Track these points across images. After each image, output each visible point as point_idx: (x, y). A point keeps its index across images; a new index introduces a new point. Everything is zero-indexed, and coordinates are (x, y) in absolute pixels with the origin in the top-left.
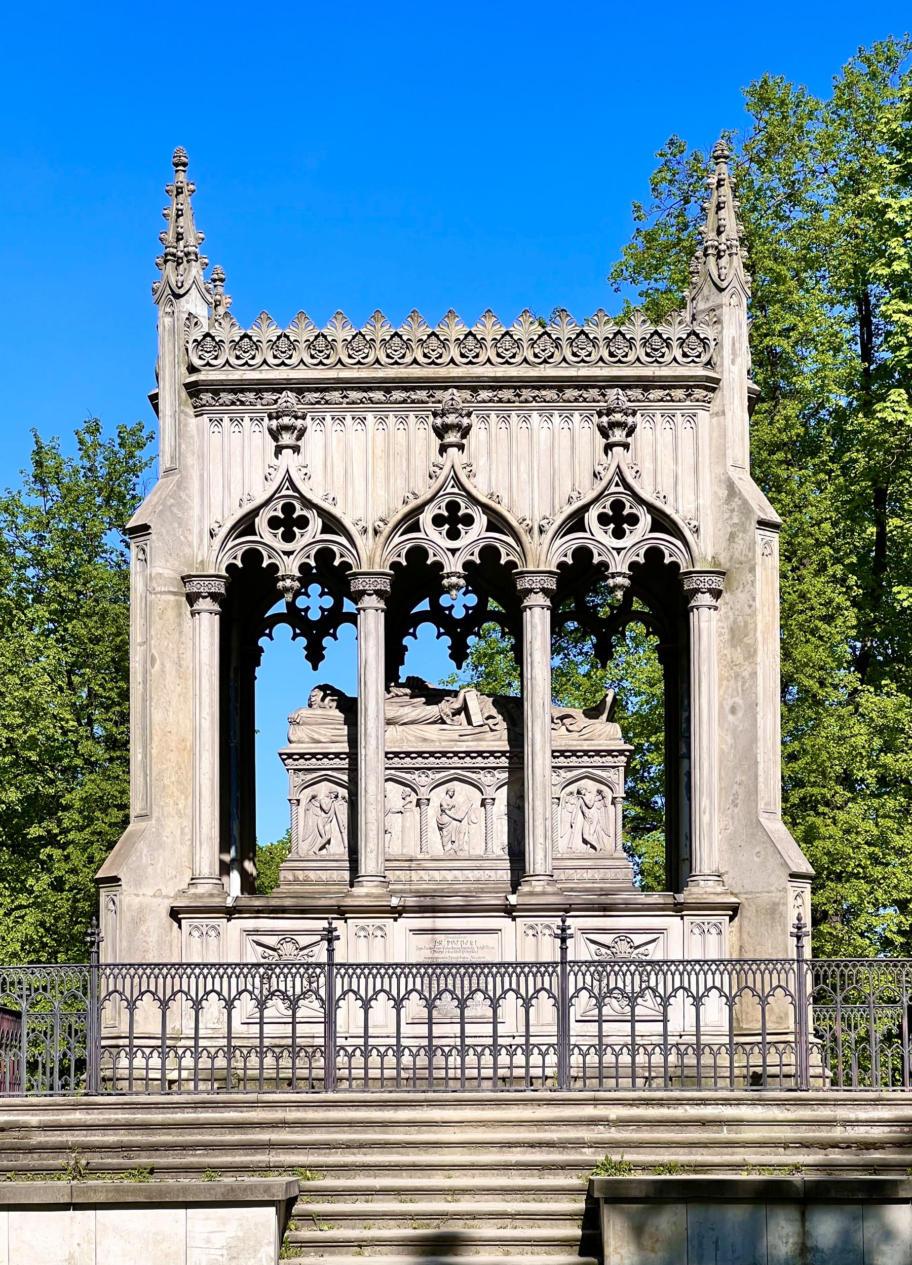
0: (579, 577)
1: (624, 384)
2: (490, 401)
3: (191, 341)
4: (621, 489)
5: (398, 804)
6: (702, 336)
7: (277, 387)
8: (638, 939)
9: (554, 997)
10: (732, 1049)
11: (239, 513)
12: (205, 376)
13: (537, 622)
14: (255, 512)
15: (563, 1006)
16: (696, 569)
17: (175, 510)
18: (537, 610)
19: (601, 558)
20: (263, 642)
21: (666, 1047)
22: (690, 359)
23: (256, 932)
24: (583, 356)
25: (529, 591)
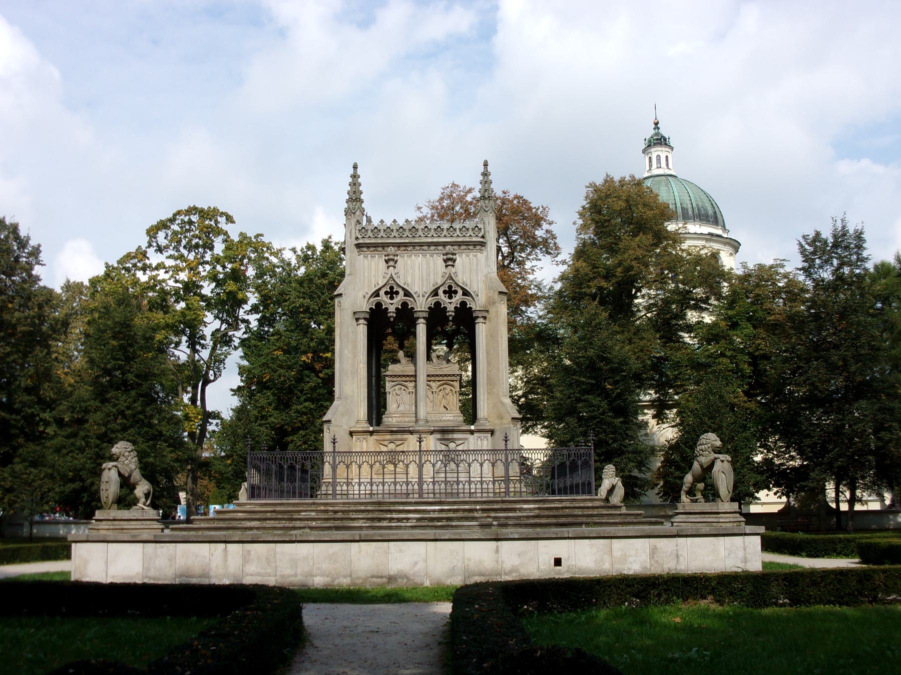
0: (436, 314)
8: (399, 443)
10: (494, 482)
12: (361, 241)
13: (421, 329)
14: (380, 289)
15: (420, 467)
25: (418, 318)
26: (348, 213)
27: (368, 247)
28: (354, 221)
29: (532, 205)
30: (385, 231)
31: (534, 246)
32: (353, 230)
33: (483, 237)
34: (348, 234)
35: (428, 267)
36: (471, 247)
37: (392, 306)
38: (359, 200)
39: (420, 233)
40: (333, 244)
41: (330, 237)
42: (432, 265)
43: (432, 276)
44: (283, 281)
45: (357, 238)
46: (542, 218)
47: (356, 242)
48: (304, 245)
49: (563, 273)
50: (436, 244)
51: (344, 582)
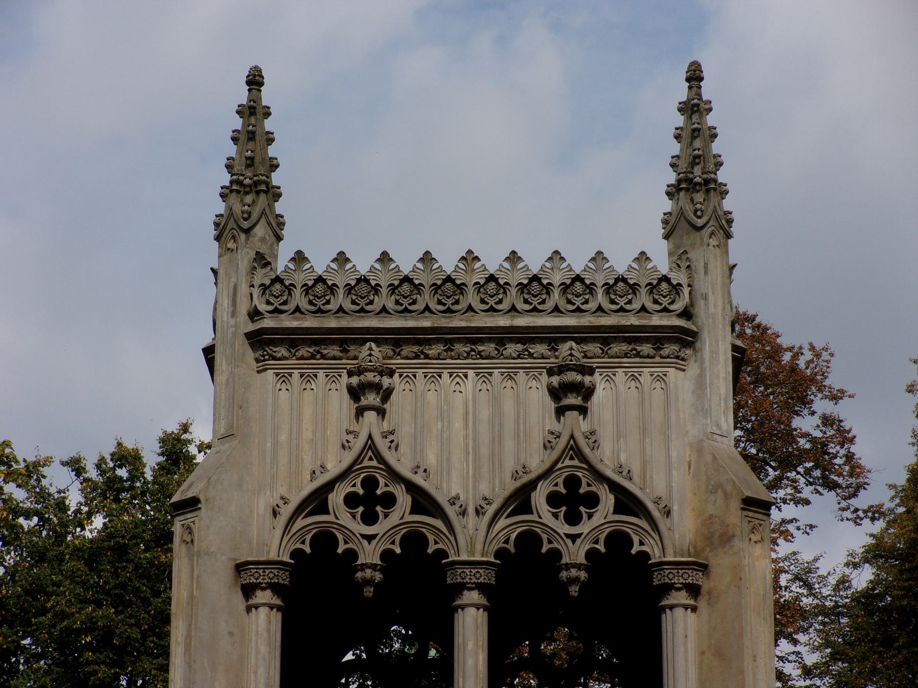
0: (522, 576)
2: (519, 357)
3: (256, 286)
4: (374, 463)
7: (362, 336)
11: (309, 488)
12: (268, 323)
13: (471, 628)
14: (329, 487)
16: (666, 559)
24: (535, 303)
26: (227, 230)
27: (293, 345)
28: (245, 258)
29: (783, 341)
30: (349, 289)
31: (788, 463)
32: (244, 289)
33: (686, 314)
34: (225, 302)
35: (497, 414)
36: (646, 348)
37: (370, 544)
38: (712, 188)
39: (471, 298)
40: (193, 449)
41: (185, 428)
42: (509, 406)
43: (509, 444)
44: (40, 556)
45: (254, 314)
46: (812, 380)
47: (251, 327)
48: (108, 449)
49: (878, 538)
50: (527, 336)
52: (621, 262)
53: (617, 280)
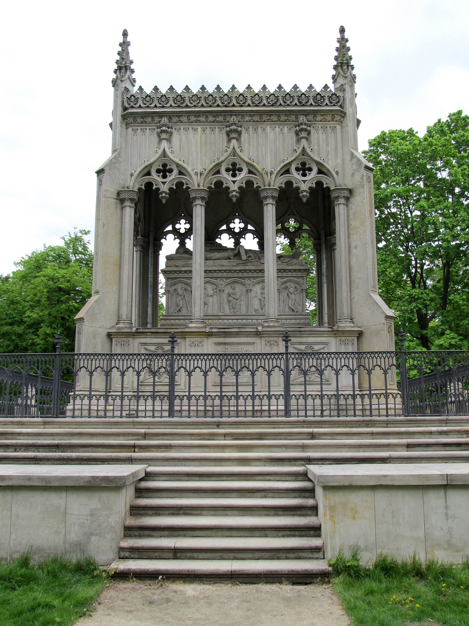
0: (217, 193)
1: (306, 113)
2: (249, 121)
5: (211, 292)
6: (338, 95)
7: (161, 115)
9: (282, 370)
15: (287, 375)
17: (116, 165)
18: (270, 206)
19: (297, 185)
20: (163, 241)
21: (306, 396)
22: (333, 104)
23: (146, 344)
25: (195, 198)
37: (164, 186)
45: (125, 109)
51: (341, 484)
52: (318, 88)
53: (317, 95)
